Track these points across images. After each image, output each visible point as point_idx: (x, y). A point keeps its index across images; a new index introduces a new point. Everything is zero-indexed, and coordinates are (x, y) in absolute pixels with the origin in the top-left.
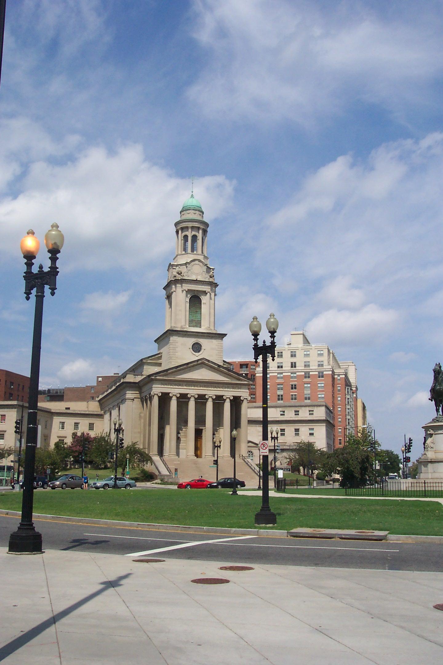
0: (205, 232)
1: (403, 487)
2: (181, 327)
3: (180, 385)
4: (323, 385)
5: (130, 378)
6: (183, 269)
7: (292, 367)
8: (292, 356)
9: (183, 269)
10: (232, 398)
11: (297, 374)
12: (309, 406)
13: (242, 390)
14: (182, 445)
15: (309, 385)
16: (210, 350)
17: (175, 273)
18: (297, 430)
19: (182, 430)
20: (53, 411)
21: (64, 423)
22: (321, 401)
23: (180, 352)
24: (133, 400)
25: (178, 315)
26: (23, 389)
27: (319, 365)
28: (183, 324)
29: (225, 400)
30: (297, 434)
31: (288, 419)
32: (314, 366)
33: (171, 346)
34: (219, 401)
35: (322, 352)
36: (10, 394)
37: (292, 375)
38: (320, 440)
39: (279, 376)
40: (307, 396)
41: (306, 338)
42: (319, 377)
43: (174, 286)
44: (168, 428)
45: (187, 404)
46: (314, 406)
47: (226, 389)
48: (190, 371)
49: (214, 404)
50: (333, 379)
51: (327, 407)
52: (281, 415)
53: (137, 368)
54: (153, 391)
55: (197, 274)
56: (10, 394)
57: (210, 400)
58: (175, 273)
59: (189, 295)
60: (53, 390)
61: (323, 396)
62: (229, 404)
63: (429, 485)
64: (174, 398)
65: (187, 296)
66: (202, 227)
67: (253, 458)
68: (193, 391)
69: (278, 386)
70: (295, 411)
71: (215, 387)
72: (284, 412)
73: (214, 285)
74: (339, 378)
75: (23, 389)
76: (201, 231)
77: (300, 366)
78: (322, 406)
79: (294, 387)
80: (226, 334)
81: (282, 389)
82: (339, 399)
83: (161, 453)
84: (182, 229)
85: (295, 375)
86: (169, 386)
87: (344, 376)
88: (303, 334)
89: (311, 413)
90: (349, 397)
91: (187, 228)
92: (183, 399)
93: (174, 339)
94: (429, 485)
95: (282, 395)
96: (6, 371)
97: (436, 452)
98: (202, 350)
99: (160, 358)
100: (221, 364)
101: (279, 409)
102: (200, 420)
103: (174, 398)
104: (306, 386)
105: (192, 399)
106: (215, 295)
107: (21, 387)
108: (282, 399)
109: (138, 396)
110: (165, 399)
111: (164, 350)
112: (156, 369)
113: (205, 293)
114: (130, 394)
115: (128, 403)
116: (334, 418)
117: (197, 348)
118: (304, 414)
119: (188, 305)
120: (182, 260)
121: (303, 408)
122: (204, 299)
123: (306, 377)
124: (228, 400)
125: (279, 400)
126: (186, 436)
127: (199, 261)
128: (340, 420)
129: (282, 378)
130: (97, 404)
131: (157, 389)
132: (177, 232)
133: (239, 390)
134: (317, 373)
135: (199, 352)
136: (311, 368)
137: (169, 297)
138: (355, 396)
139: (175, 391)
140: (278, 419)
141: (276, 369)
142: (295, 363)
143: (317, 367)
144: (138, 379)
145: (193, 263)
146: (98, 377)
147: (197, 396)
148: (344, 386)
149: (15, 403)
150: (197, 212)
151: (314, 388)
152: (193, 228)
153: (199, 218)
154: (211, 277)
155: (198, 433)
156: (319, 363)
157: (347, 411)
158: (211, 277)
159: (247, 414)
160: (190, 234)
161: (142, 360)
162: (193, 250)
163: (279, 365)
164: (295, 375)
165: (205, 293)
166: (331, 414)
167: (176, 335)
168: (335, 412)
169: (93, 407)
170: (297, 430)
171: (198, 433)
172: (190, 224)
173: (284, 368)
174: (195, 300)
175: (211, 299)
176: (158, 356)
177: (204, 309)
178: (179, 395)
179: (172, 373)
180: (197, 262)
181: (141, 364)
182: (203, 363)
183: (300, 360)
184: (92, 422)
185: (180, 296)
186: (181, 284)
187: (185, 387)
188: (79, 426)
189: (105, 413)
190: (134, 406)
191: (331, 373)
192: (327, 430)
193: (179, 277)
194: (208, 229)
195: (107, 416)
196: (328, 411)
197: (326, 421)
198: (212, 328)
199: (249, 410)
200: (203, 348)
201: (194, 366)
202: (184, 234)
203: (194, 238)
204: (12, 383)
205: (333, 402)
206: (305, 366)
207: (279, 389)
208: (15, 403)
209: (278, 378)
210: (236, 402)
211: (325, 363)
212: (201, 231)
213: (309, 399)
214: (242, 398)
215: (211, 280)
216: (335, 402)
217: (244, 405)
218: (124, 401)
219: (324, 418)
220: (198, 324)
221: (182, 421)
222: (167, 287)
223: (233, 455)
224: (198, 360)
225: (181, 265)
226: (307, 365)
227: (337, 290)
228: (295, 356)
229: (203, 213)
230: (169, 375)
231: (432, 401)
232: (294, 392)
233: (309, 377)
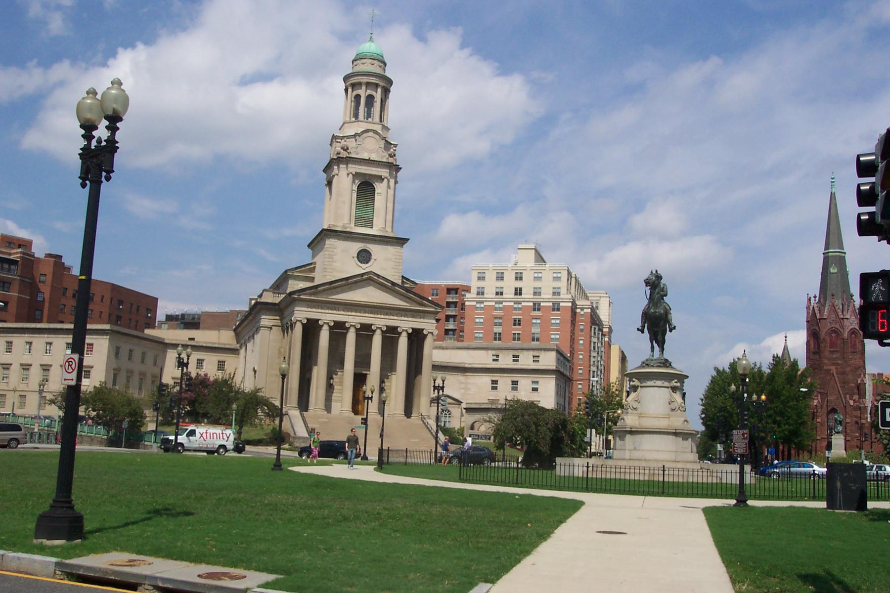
0: (386, 91)
1: (579, 472)
2: (344, 226)
3: (335, 309)
4: (558, 321)
5: (269, 298)
6: (351, 143)
7: (516, 294)
8: (516, 278)
9: (351, 143)
10: (410, 331)
11: (523, 304)
12: (533, 349)
13: (426, 320)
14: (335, 395)
15: (539, 321)
16: (385, 262)
17: (339, 149)
18: (515, 383)
19: (336, 375)
20: (166, 341)
21: (31, 343)
22: (553, 344)
23: (340, 260)
24: (271, 328)
25: (339, 207)
26: (138, 310)
27: (554, 294)
28: (346, 221)
29: (400, 334)
30: (515, 389)
31: (523, 367)
32: (547, 295)
33: (327, 253)
34: (391, 335)
35: (559, 275)
36: (117, 316)
37: (516, 306)
38: (546, 395)
39: (497, 306)
40: (536, 336)
41: (539, 254)
42: (554, 310)
43: (336, 167)
44: (315, 370)
45: (370, 338)
46: (541, 350)
47: (403, 318)
48: (350, 290)
49: (358, 336)
50: (574, 314)
51: (559, 352)
52: (494, 360)
53: (279, 285)
54: (295, 315)
55: (371, 152)
56: (117, 316)
57: (378, 332)
58: (339, 149)
59: (357, 181)
60: (189, 315)
61: (558, 337)
62: (406, 339)
63: (623, 470)
64: (326, 328)
65: (354, 182)
66: (382, 84)
67: (451, 419)
68: (354, 319)
69: (496, 321)
70: (514, 356)
71: (387, 314)
72: (498, 356)
73: (395, 168)
74: (582, 313)
75: (138, 310)
76: (379, 90)
77: (527, 294)
78: (552, 350)
79: (517, 322)
80: (408, 240)
81: (500, 324)
82: (581, 342)
83: (303, 404)
84: (354, 86)
85: (520, 306)
86: (319, 310)
87: (589, 311)
88: (536, 250)
89: (536, 359)
90: (595, 340)
91: (359, 84)
92: (339, 330)
93: (330, 242)
94: (623, 470)
95: (500, 334)
96: (113, 284)
97: (640, 416)
98: (372, 261)
99: (313, 270)
100: (399, 282)
101: (491, 352)
102: (363, 360)
103: (326, 328)
104: (534, 321)
105: (352, 330)
106: (396, 182)
107: (135, 307)
108: (500, 339)
109: (279, 323)
110: (311, 329)
111: (318, 259)
112: (302, 285)
113: (380, 179)
114: (266, 320)
115: (263, 332)
116: (572, 369)
117: (364, 256)
118: (526, 361)
119: (355, 195)
120: (350, 131)
121: (525, 353)
122: (380, 188)
123: (534, 310)
124: (404, 334)
125: (495, 339)
126: (341, 383)
127: (375, 132)
128: (581, 371)
129: (501, 309)
130: (232, 333)
131: (301, 314)
132: (346, 90)
133: (422, 320)
134: (551, 304)
135: (367, 263)
136: (542, 296)
137: (329, 183)
138: (606, 339)
139: (327, 317)
140: (488, 366)
141: (494, 296)
142: (521, 289)
143: (550, 296)
144: (277, 299)
145: (365, 135)
146: (251, 299)
147: (385, 329)
148: (589, 325)
149: (107, 327)
150: (376, 62)
151: (546, 325)
152: (368, 84)
153: (378, 71)
154: (390, 156)
155: (360, 379)
156: (555, 290)
157: (592, 359)
158: (390, 156)
159: (431, 356)
160: (363, 92)
161: (286, 271)
162: (369, 115)
163: (498, 290)
164: (520, 306)
165: (380, 179)
166: (567, 363)
167: (330, 237)
168: (575, 361)
169: (226, 337)
170: (515, 383)
171: (360, 379)
172: (364, 79)
173: (504, 296)
174: (366, 188)
175: (389, 187)
176: (310, 268)
177: (379, 201)
178: (332, 324)
179: (324, 290)
180: (371, 134)
181: (285, 277)
182: (370, 279)
183: (528, 286)
184: (222, 359)
185: (344, 180)
186: (347, 164)
187: (342, 312)
188: (204, 364)
189: (241, 347)
190: (272, 337)
191: (570, 304)
192: (557, 385)
193: (344, 154)
194: (391, 89)
195: (242, 351)
196: (562, 358)
197: (558, 373)
198: (389, 229)
199: (435, 352)
200: (373, 257)
201: (356, 282)
202: (355, 93)
203: (370, 99)
204: (121, 302)
205: (572, 347)
206: (535, 294)
207: (496, 324)
208: (107, 327)
209: (496, 309)
210: (417, 338)
211: (563, 291)
212: (379, 90)
213: (538, 340)
214: (425, 332)
215: (391, 160)
216: (575, 346)
217: (428, 343)
218: (257, 330)
219: (554, 368)
220: (369, 223)
221: (336, 360)
222: (328, 169)
223: (408, 412)
224: (363, 275)
225: (348, 137)
226: (537, 293)
227: (663, 216)
228: (521, 279)
229: (385, 65)
230: (323, 293)
231: (643, 332)
232: (517, 330)
233: (539, 310)
